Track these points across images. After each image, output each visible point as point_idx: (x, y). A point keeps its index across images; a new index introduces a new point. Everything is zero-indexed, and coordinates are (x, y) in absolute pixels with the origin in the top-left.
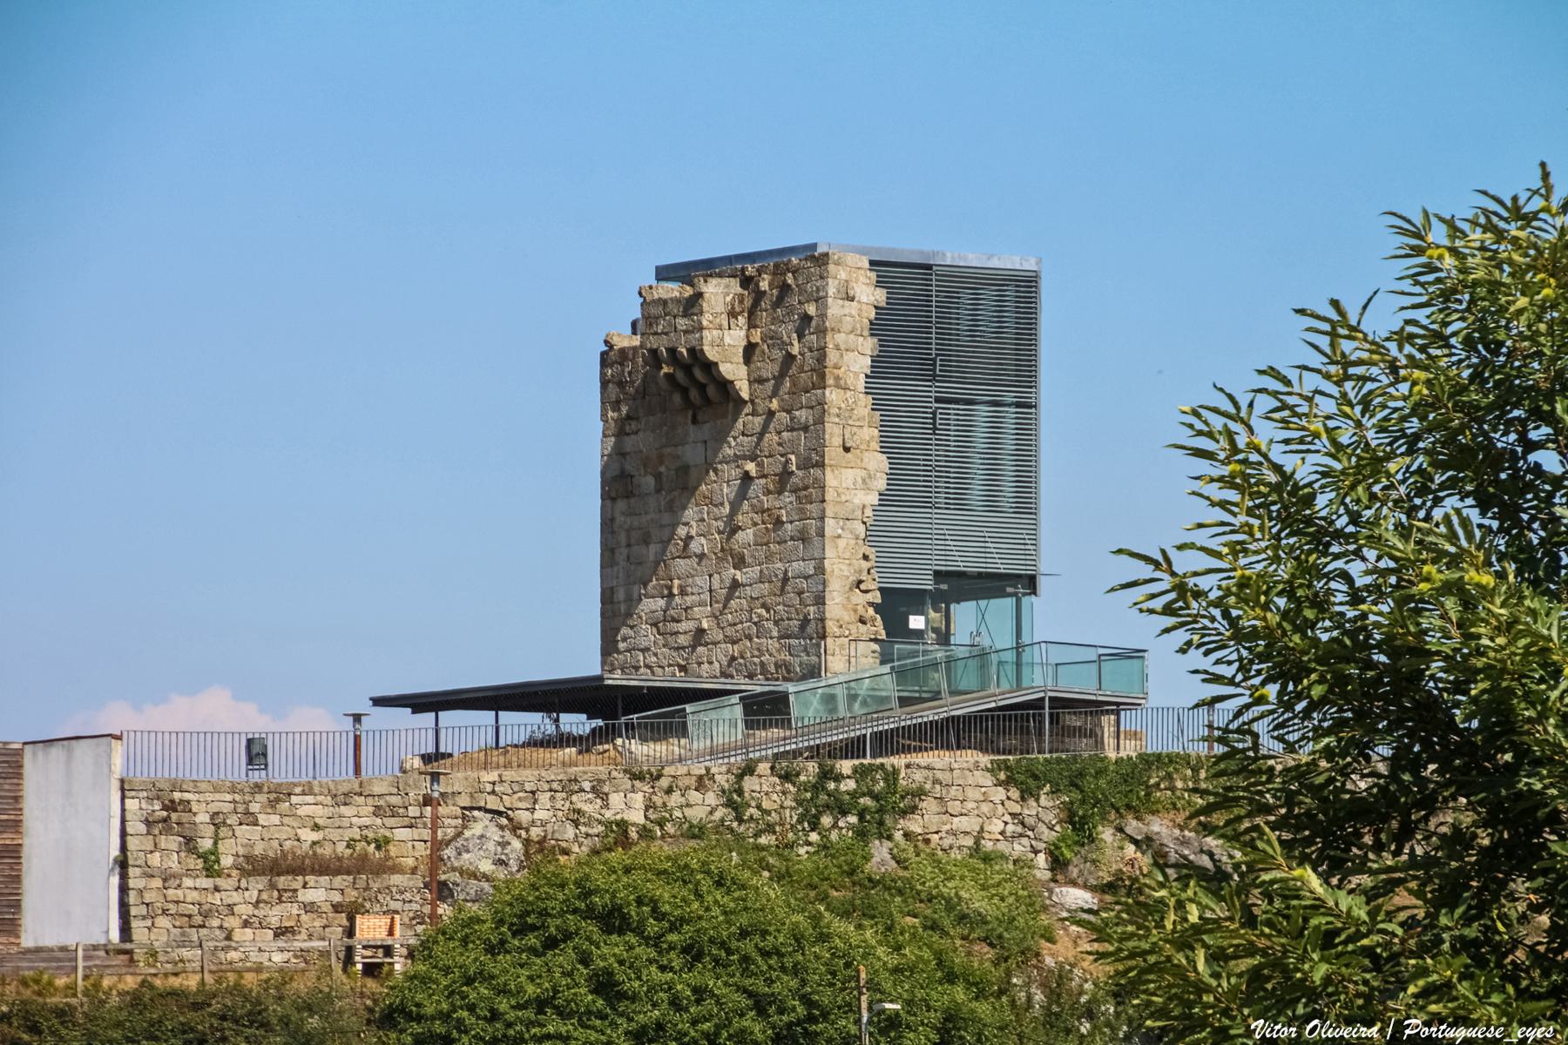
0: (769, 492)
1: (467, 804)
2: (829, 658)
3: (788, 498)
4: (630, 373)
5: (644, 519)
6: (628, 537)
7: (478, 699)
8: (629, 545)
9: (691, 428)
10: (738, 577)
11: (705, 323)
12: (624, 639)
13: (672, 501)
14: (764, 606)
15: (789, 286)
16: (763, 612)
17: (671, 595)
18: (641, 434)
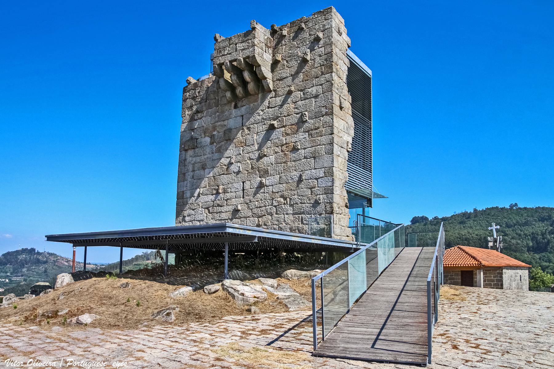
0: (287, 134)
1: (154, 350)
2: (335, 229)
3: (301, 136)
4: (199, 92)
5: (203, 158)
6: (194, 167)
7: (140, 239)
8: (193, 171)
9: (234, 111)
10: (264, 181)
11: (256, 43)
12: (189, 215)
13: (220, 147)
14: (282, 196)
15: (303, 28)
16: (282, 200)
17: (218, 193)
18: (204, 119)
